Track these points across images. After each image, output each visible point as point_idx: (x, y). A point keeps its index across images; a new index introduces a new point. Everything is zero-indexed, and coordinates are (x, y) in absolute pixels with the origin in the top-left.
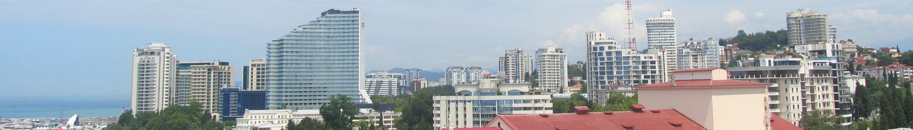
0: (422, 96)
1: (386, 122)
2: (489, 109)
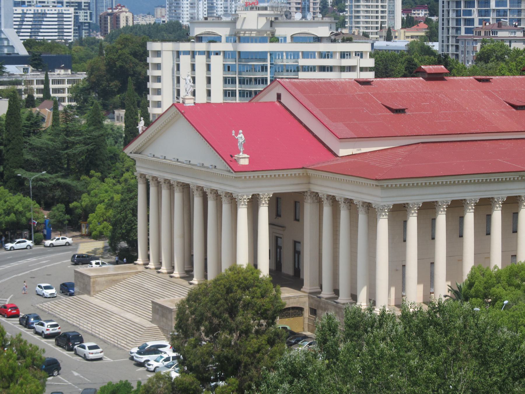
0: (125, 42)
1: (56, 91)
2: (254, 69)
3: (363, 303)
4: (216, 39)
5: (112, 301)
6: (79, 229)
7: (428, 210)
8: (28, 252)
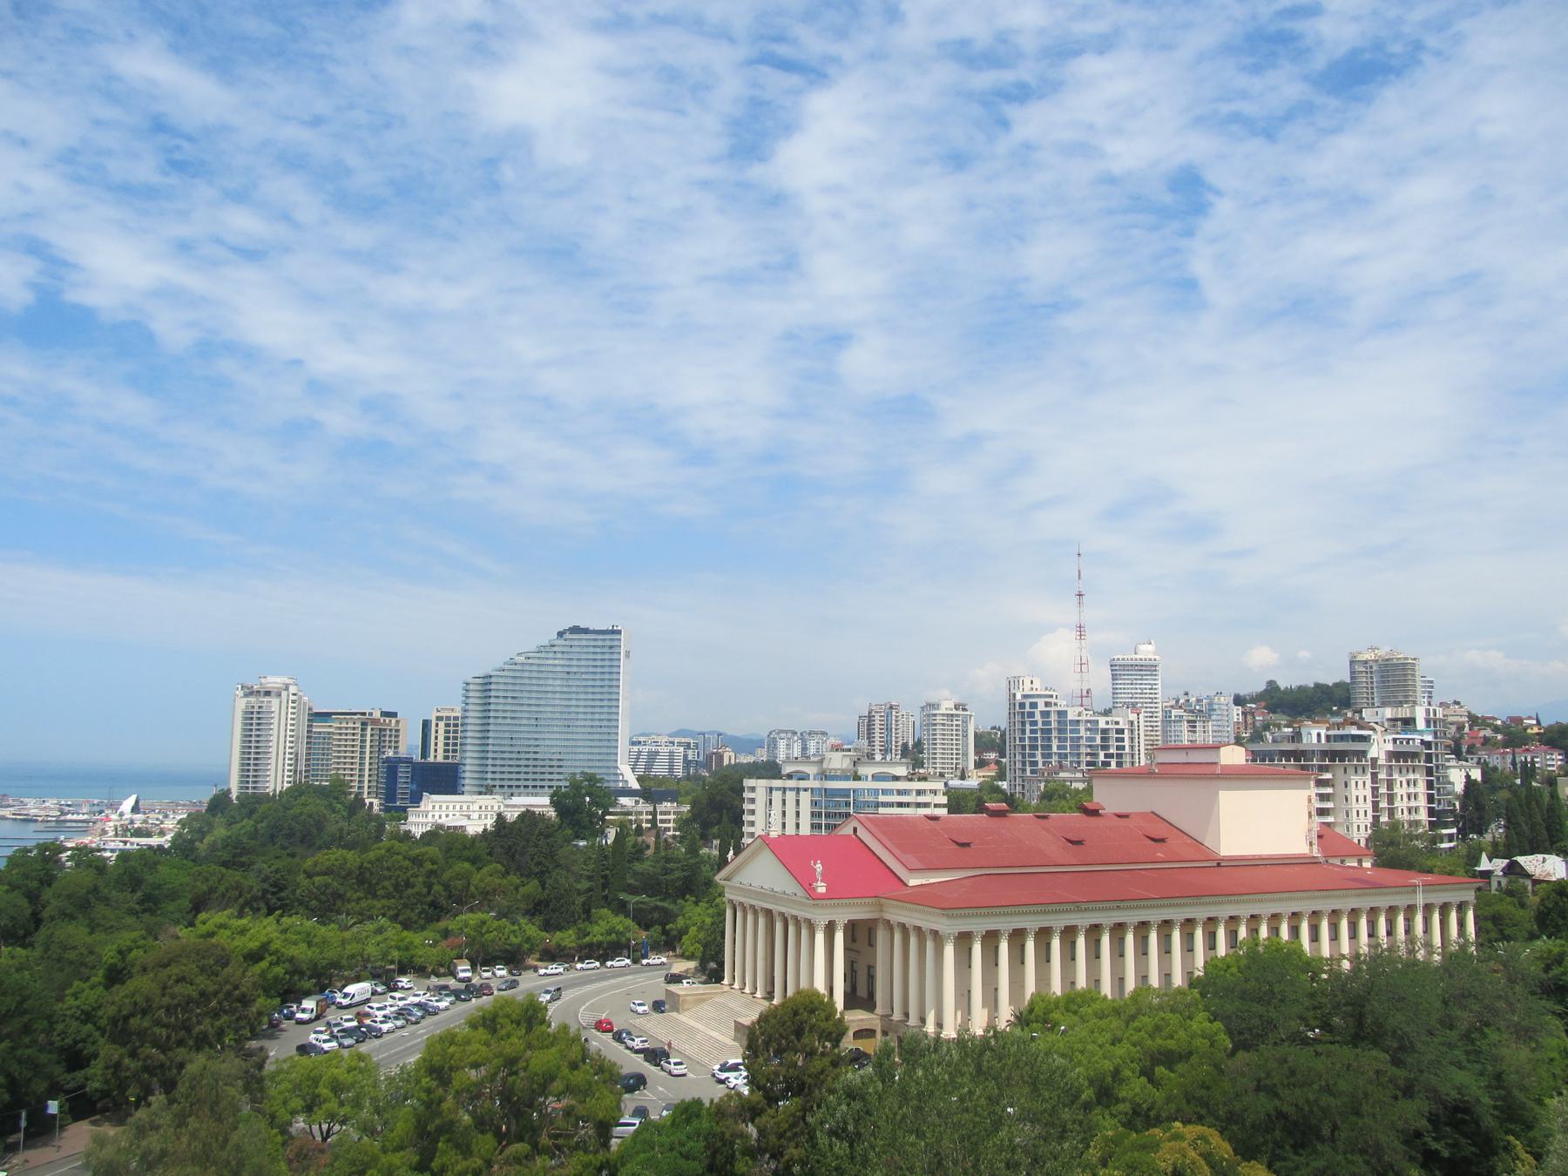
1: (662, 821)
3: (930, 1028)
4: (804, 777)
5: (699, 1019)
6: (674, 950)
7: (1017, 937)
8: (626, 970)
